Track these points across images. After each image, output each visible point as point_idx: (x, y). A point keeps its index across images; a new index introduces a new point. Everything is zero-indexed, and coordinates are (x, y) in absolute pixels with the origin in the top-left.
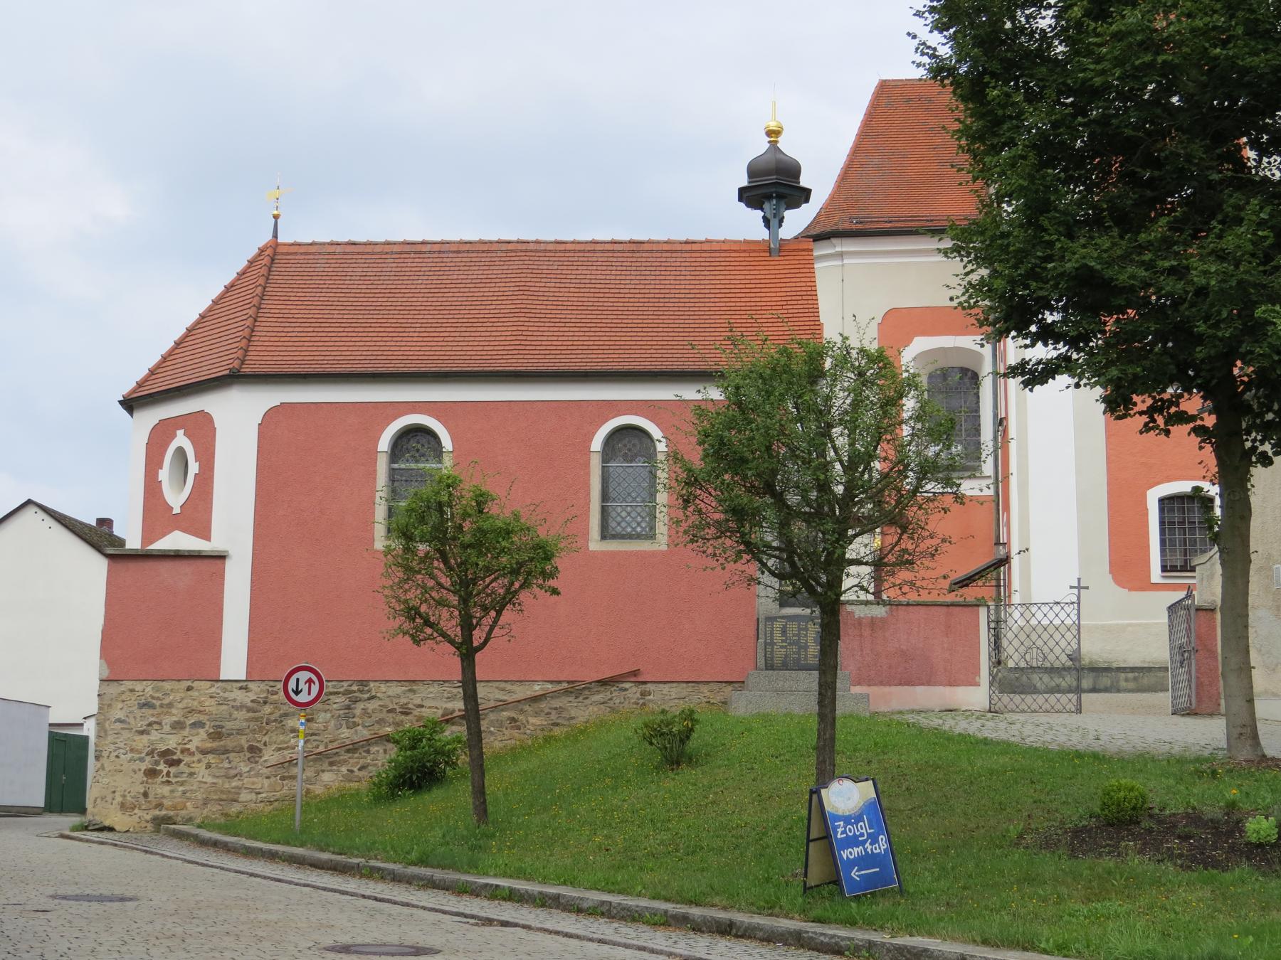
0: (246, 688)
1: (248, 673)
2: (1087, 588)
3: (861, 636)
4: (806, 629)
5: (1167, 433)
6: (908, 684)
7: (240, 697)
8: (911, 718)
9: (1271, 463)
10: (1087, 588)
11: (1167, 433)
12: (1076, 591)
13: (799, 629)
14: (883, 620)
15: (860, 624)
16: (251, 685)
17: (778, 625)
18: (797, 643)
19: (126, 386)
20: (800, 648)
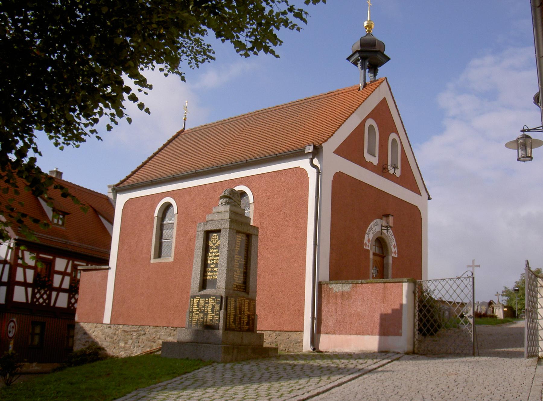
0: (110, 327)
1: (111, 321)
2: (479, 266)
3: (336, 303)
4: (208, 303)
5: (166, 75)
6: (360, 334)
7: (107, 330)
8: (48, 367)
9: (141, 110)
10: (479, 266)
11: (166, 75)
12: (471, 269)
13: (205, 303)
14: (349, 293)
15: (336, 296)
16: (112, 326)
17: (196, 300)
18: (203, 312)
19: (84, 143)
20: (205, 314)
